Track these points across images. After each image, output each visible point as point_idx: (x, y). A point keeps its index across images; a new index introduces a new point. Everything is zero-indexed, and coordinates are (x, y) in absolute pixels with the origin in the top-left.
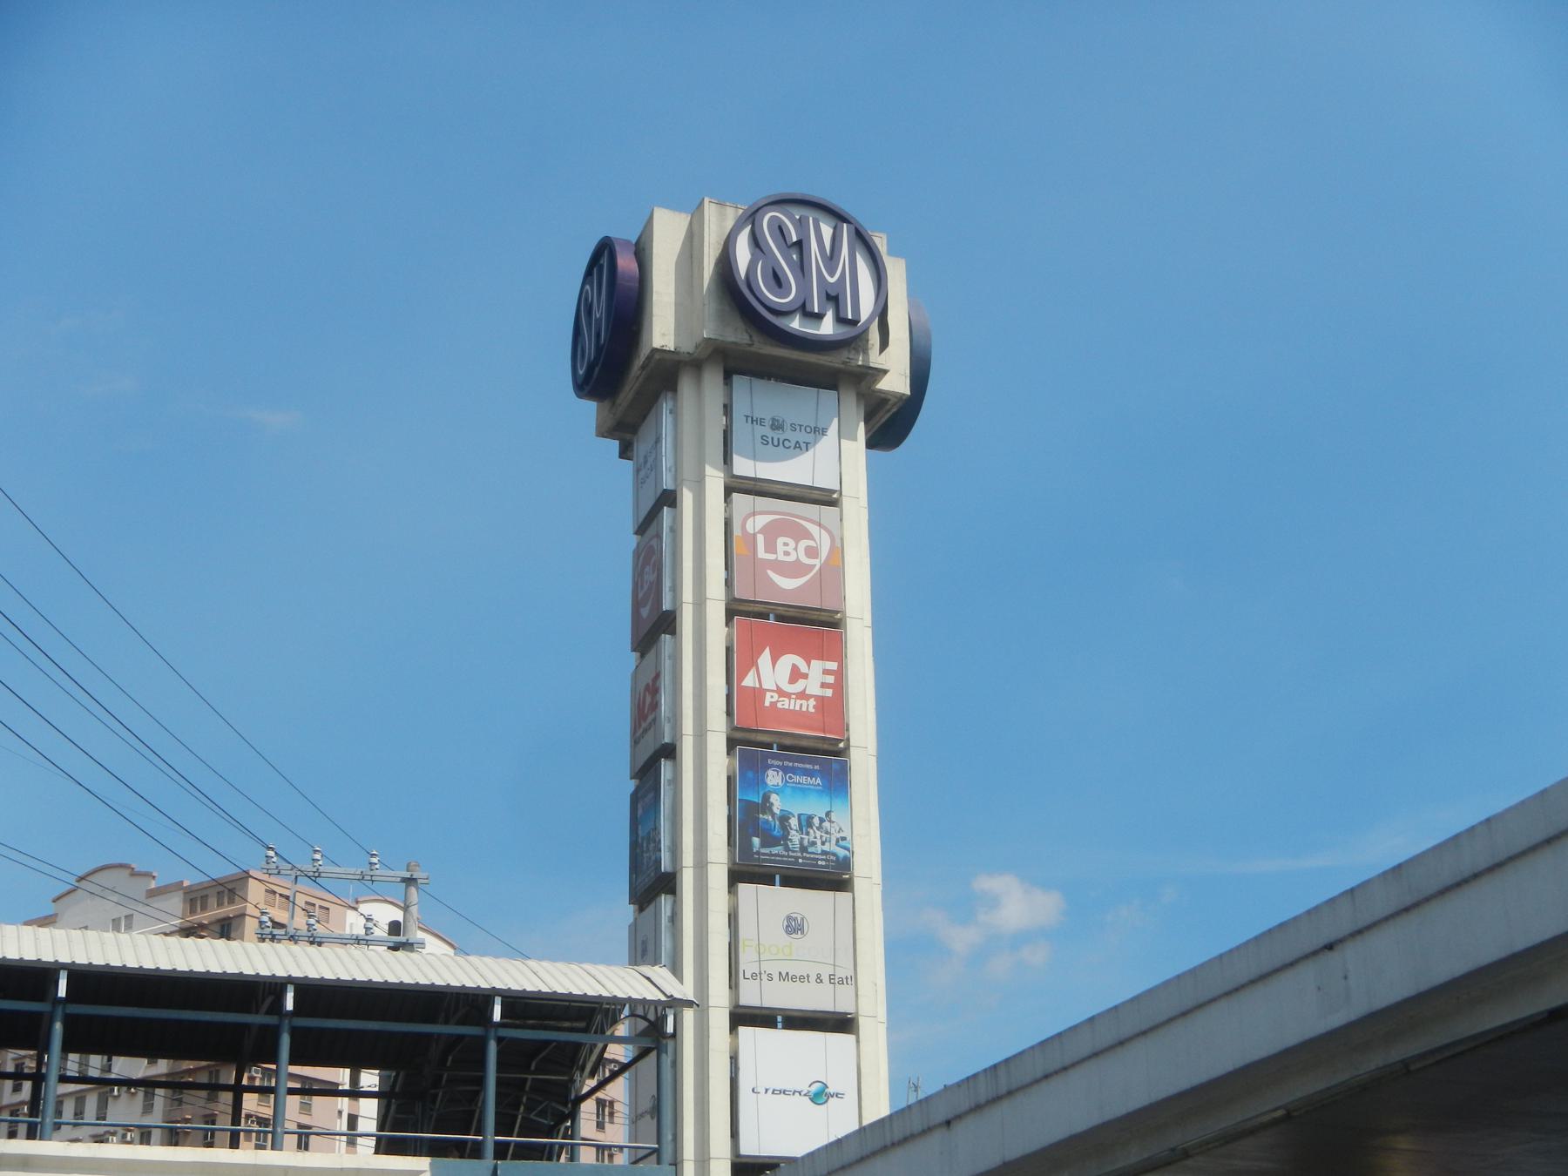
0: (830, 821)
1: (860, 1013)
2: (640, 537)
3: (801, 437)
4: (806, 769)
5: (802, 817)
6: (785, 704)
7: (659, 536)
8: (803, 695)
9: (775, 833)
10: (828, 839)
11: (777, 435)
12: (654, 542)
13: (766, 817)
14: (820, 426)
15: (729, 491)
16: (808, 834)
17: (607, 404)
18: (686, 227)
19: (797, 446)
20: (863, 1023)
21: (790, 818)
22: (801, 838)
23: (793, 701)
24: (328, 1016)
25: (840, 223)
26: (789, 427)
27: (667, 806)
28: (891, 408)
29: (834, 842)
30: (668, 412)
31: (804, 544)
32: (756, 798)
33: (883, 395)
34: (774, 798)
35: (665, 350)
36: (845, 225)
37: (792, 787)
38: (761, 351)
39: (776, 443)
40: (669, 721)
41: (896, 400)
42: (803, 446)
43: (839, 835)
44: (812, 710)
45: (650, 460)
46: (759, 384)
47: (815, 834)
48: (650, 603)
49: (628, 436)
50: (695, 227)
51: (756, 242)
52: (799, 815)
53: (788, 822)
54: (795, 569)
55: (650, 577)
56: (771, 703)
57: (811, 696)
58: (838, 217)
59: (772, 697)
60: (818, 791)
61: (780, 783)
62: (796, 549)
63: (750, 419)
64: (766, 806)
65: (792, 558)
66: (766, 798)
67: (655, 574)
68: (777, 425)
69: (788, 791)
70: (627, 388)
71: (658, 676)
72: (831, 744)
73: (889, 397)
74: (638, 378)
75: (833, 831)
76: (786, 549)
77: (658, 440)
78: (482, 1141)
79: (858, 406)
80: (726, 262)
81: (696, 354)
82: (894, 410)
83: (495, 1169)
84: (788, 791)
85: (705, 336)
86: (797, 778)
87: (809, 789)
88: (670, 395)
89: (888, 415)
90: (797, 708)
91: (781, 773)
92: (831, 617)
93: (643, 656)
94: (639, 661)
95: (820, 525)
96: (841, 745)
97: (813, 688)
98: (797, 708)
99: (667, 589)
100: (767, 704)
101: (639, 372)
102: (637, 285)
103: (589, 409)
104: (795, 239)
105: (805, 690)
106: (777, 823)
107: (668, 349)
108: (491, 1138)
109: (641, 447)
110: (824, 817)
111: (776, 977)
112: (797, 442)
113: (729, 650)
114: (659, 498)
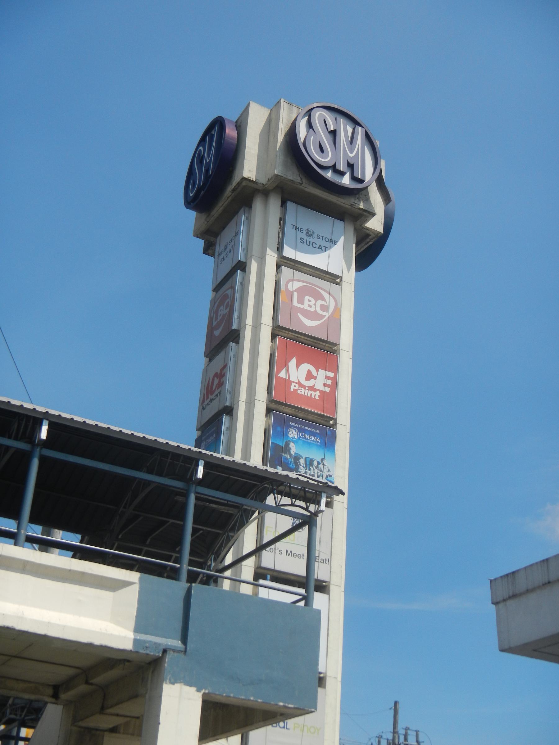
0: (323, 464)
1: (331, 582)
2: (215, 293)
3: (323, 243)
4: (311, 431)
5: (307, 459)
6: (302, 391)
7: (233, 288)
8: (312, 388)
9: (291, 466)
10: (321, 475)
11: (309, 239)
12: (229, 292)
13: (286, 455)
14: (334, 239)
15: (278, 267)
16: (310, 470)
17: (203, 216)
18: (262, 124)
19: (320, 247)
20: (332, 588)
21: (300, 459)
22: (306, 471)
23: (307, 391)
24: (72, 453)
25: (357, 126)
26: (316, 236)
27: (224, 445)
28: (369, 242)
29: (324, 477)
30: (245, 218)
31: (319, 302)
32: (281, 443)
33: (367, 231)
34: (292, 445)
35: (250, 180)
36: (360, 127)
37: (303, 440)
38: (306, 190)
39: (308, 244)
40: (230, 393)
41: (374, 236)
42: (323, 248)
43: (328, 474)
44: (317, 398)
45: (229, 247)
46: (301, 209)
47: (314, 471)
48: (221, 328)
49: (212, 239)
50: (273, 116)
51: (310, 125)
52: (306, 458)
53: (298, 461)
54: (314, 316)
55: (223, 311)
56: (294, 389)
57: (317, 390)
58: (355, 122)
59: (295, 386)
60: (318, 445)
61: (296, 437)
62: (315, 304)
63: (294, 227)
64: (287, 449)
65: (312, 309)
66: (287, 444)
67: (228, 310)
68: (309, 234)
69: (300, 442)
70: (220, 204)
71: (225, 366)
72: (326, 421)
73: (371, 233)
74: (228, 197)
75: (324, 471)
76: (310, 303)
77: (237, 234)
78: (179, 568)
79: (354, 235)
80: (292, 133)
81: (266, 186)
82: (371, 243)
83: (189, 590)
84: (300, 442)
85: (276, 173)
86: (306, 436)
87: (312, 443)
88: (247, 209)
89: (368, 245)
90: (309, 395)
91: (297, 431)
92: (331, 348)
93: (210, 360)
94: (208, 363)
95: (330, 294)
96: (331, 422)
97: (319, 386)
98: (309, 395)
99: (236, 317)
100: (292, 389)
101: (231, 193)
102: (236, 142)
103: (192, 215)
104: (332, 129)
105: (314, 385)
106: (293, 460)
107: (252, 179)
108: (185, 567)
109: (219, 248)
110: (320, 461)
111: (284, 552)
112: (320, 245)
113: (272, 356)
114: (234, 266)
